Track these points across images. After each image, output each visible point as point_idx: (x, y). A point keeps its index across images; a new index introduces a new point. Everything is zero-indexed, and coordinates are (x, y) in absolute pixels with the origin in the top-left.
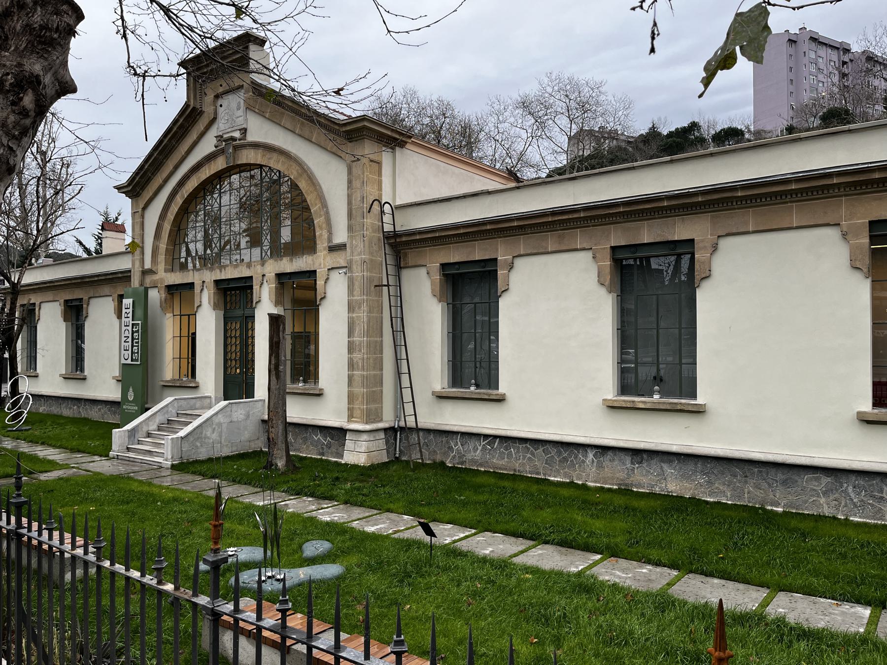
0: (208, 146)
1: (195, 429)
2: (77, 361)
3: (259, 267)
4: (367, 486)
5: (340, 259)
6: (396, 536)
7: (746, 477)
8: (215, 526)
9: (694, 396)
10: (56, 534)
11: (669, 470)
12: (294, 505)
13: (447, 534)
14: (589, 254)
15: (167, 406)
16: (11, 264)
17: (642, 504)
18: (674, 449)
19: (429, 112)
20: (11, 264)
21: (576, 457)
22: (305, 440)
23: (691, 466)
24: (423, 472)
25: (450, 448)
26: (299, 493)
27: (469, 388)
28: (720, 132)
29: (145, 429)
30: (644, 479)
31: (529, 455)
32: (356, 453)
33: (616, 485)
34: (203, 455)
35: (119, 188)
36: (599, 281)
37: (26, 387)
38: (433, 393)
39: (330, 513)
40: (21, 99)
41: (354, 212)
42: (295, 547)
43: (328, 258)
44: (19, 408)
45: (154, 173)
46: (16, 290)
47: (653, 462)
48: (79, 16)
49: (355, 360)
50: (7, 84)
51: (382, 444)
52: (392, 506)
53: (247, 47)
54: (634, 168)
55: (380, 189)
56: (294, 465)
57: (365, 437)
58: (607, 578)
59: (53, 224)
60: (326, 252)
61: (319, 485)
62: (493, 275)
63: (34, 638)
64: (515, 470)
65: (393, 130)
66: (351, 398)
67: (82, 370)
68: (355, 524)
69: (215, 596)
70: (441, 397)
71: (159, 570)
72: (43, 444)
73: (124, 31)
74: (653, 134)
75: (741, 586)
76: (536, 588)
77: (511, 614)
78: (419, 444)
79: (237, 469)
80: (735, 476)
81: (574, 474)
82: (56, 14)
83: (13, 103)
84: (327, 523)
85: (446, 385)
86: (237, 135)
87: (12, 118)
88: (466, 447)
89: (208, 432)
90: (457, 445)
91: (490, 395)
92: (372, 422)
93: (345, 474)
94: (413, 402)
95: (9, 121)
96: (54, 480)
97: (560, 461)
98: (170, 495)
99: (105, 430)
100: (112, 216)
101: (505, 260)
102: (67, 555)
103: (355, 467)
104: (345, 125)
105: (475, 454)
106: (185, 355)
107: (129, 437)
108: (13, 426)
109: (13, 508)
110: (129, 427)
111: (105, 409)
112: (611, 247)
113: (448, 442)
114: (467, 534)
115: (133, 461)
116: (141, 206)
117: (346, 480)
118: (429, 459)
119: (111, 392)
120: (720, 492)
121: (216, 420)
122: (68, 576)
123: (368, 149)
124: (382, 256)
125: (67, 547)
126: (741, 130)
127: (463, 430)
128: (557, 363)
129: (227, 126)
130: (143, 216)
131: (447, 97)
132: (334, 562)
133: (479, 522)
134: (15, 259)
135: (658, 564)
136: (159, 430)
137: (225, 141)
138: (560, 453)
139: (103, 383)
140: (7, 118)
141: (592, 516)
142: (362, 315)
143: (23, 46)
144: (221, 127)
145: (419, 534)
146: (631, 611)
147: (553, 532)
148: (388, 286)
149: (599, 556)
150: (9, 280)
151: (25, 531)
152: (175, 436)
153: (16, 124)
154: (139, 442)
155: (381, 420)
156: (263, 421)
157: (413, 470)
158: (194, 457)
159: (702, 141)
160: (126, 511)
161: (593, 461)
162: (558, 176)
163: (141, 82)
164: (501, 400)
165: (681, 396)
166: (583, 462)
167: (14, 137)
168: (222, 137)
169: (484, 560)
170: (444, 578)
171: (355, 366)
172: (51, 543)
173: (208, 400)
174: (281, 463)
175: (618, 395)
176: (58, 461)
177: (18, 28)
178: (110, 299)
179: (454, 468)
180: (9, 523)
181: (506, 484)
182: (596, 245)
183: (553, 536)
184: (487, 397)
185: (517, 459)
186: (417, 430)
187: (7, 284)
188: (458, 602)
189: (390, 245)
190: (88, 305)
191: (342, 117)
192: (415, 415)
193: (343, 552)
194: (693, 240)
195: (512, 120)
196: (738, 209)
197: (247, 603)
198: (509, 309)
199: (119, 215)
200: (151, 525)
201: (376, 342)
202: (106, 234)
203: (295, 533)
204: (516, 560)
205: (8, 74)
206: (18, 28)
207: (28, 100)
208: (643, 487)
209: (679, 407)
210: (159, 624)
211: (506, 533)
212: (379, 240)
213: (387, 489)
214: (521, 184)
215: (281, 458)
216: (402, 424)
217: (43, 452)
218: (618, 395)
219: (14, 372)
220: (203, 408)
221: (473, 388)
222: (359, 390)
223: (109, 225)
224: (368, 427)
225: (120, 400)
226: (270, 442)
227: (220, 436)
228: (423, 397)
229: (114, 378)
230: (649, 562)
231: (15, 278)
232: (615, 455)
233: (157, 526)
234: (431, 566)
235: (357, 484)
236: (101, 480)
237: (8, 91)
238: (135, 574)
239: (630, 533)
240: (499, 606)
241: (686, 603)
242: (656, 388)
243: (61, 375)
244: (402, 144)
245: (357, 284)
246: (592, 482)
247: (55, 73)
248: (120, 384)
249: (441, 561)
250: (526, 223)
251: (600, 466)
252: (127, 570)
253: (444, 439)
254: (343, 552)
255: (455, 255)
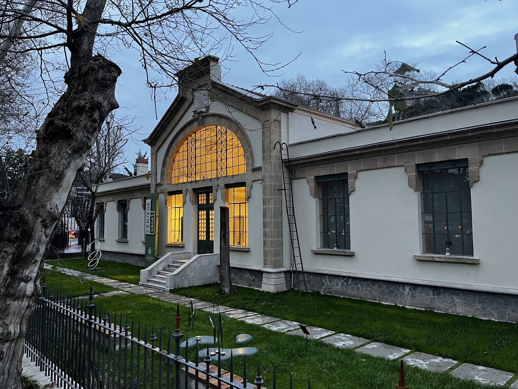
0: (189, 116)
1: (182, 270)
2: (124, 232)
3: (216, 181)
4: (272, 305)
5: (258, 175)
6: (288, 333)
7: (507, 304)
8: (177, 319)
9: (472, 254)
10: (113, 325)
11: (457, 300)
12: (237, 314)
13: (318, 334)
14: (403, 169)
15: (168, 257)
16: (92, 181)
17: (440, 320)
18: (460, 287)
19: (312, 88)
20: (92, 181)
21: (398, 290)
22: (241, 277)
23: (471, 297)
24: (305, 297)
25: (323, 284)
26: (236, 307)
27: (333, 248)
28: (497, 87)
29: (157, 270)
30: (442, 305)
31: (369, 289)
32: (269, 285)
33: (424, 308)
34: (186, 285)
35: (145, 141)
36: (409, 185)
37: (99, 246)
38: (312, 251)
39: (254, 319)
40: (93, 114)
41: (266, 149)
42: (232, 337)
43: (252, 175)
44: (95, 258)
45: (162, 133)
46: (94, 196)
47: (447, 294)
48: (119, 72)
49: (267, 232)
50: (87, 108)
51: (283, 280)
52: (287, 316)
53: (209, 64)
54: (428, 118)
55: (280, 136)
56: (234, 291)
57: (273, 276)
58: (412, 364)
59: (113, 160)
60: (251, 172)
61: (247, 303)
62: (345, 182)
63: (96, 376)
64: (361, 298)
65: (287, 103)
66: (265, 254)
67: (126, 238)
68: (265, 326)
69: (177, 354)
70: (317, 253)
71: (153, 340)
72: (106, 277)
73: (145, 65)
74: (454, 89)
75: (496, 371)
76: (367, 367)
77: (350, 382)
78: (304, 280)
79: (204, 293)
80: (500, 304)
81: (398, 301)
82: (109, 72)
83: (90, 117)
84: (250, 324)
85: (320, 247)
86: (204, 110)
87: (89, 124)
88: (332, 283)
89: (189, 272)
90: (327, 282)
91: (345, 252)
92: (277, 268)
93: (262, 297)
94: (300, 256)
95: (88, 125)
96: (111, 297)
97: (388, 293)
98: (169, 306)
99: (136, 270)
100: (143, 155)
101: (352, 173)
102: (117, 336)
103: (268, 293)
104: (262, 101)
105: (337, 287)
106: (177, 229)
107: (149, 274)
108: (92, 267)
109: (88, 310)
110: (148, 269)
111: (137, 259)
112: (416, 164)
113: (321, 280)
114: (330, 334)
115: (149, 287)
116: (156, 150)
117: (263, 301)
118: (311, 290)
119: (140, 250)
120: (491, 314)
121: (193, 265)
122: (117, 347)
123: (274, 114)
124: (282, 174)
125: (118, 331)
126: (510, 86)
127: (330, 273)
128: (386, 233)
129: (200, 105)
130: (156, 155)
131: (322, 79)
132: (252, 346)
133: (337, 327)
134: (94, 178)
135: (445, 357)
136: (164, 271)
137: (198, 113)
138: (388, 288)
139: (136, 246)
140: (87, 124)
141: (407, 326)
142: (271, 206)
143: (94, 88)
144: (196, 106)
145: (301, 333)
146: (424, 383)
147: (381, 335)
148: (285, 189)
149: (409, 351)
150: (91, 191)
151: (93, 321)
152: (171, 274)
153: (91, 126)
154: (154, 277)
155: (283, 267)
156: (218, 266)
157: (301, 296)
158: (181, 286)
159: (485, 93)
160: (144, 314)
161: (409, 293)
162: (390, 122)
163: (154, 90)
164: (352, 255)
165: (464, 254)
166: (403, 293)
167: (90, 132)
168: (196, 111)
169: (338, 349)
170: (314, 359)
171: (267, 235)
172: (105, 327)
173: (189, 254)
174: (227, 290)
175: (424, 253)
176: (118, 287)
177: (92, 80)
178: (140, 199)
179: (325, 295)
180: (86, 317)
181: (356, 306)
182: (406, 163)
183: (381, 337)
184: (343, 254)
185: (363, 291)
186: (303, 272)
187: (90, 193)
188: (321, 373)
189: (286, 166)
190: (129, 202)
191: (258, 97)
192: (302, 264)
193: (258, 341)
194: (467, 159)
195: (361, 89)
196: (495, 139)
197: (202, 367)
198: (355, 202)
199: (146, 154)
200: (158, 322)
201: (279, 221)
202: (140, 164)
203: (232, 330)
204: (358, 350)
205: (87, 103)
206: (92, 80)
207: (96, 115)
208: (441, 310)
209: (462, 261)
210: (160, 375)
211: (353, 334)
212: (280, 164)
213: (285, 306)
214: (364, 129)
215: (227, 287)
216: (294, 269)
217: (105, 281)
218: (424, 253)
219: (93, 239)
220: (186, 259)
221: (335, 248)
222: (269, 249)
223: (141, 160)
224: (275, 270)
225: (144, 254)
226: (222, 278)
227: (195, 274)
228: (306, 254)
229: (142, 242)
230: (440, 355)
231: (94, 189)
232: (423, 289)
233: (161, 323)
234: (306, 351)
235: (269, 303)
236: (134, 297)
237: (87, 111)
238: (142, 343)
239: (430, 338)
240: (344, 376)
241: (459, 379)
242: (447, 249)
243: (116, 240)
244: (292, 110)
245: (268, 189)
246: (408, 306)
247: (109, 100)
248: (145, 245)
249: (312, 348)
250: (364, 152)
251: (413, 296)
252: (139, 340)
253: (319, 278)
254: (258, 341)
255: (323, 171)
